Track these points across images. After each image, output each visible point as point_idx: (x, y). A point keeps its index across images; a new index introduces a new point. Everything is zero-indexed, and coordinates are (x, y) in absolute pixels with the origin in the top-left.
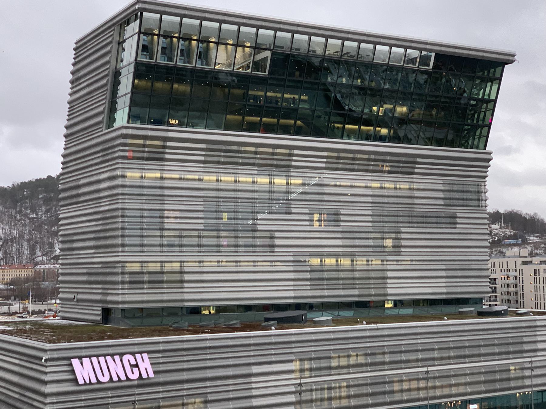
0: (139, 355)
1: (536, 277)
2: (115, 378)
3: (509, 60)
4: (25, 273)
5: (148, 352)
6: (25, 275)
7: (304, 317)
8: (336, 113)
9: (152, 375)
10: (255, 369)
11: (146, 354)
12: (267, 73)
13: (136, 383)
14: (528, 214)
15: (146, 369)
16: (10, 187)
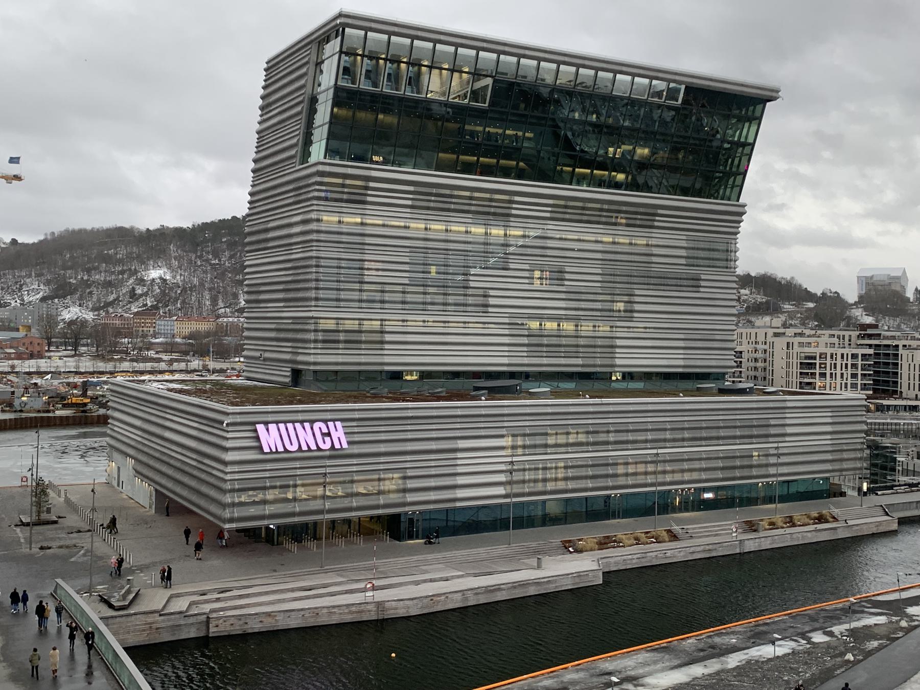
0: (332, 423)
1: (788, 351)
2: (305, 448)
3: (772, 97)
4: (206, 326)
5: (342, 420)
9: (345, 445)
10: (462, 444)
11: (339, 422)
12: (487, 105)
13: (328, 453)
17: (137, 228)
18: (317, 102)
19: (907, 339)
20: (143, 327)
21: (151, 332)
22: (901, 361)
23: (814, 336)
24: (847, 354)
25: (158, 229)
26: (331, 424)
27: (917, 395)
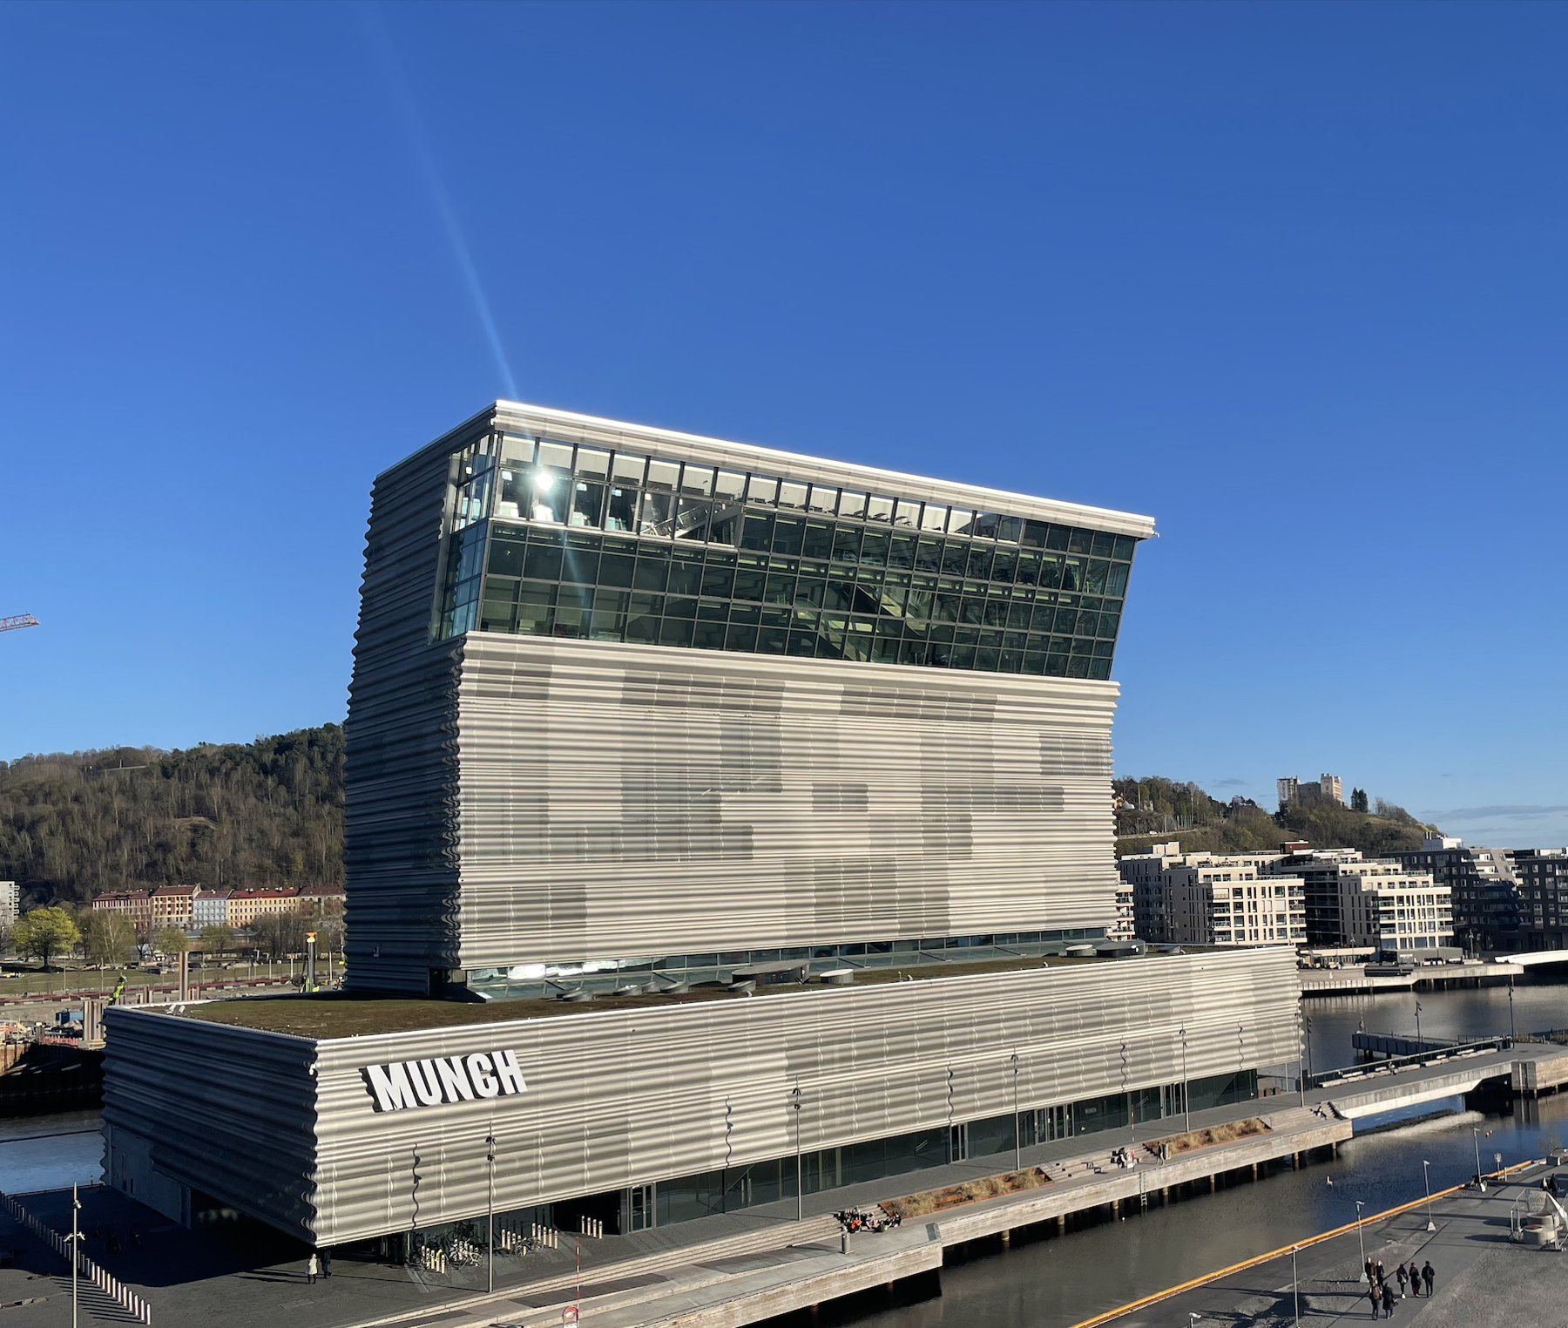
1: (1191, 888)
4: (283, 906)
6: (282, 909)
7: (803, 972)
8: (830, 614)
11: (512, 1051)
13: (493, 1104)
14: (1180, 785)
15: (512, 1077)
16: (251, 746)
17: (157, 750)
18: (461, 543)
19: (1347, 863)
20: (169, 913)
21: (185, 920)
22: (1343, 919)
23: (1222, 865)
24: (1270, 888)
25: (195, 749)
26: (497, 1056)
27: (1365, 940)
